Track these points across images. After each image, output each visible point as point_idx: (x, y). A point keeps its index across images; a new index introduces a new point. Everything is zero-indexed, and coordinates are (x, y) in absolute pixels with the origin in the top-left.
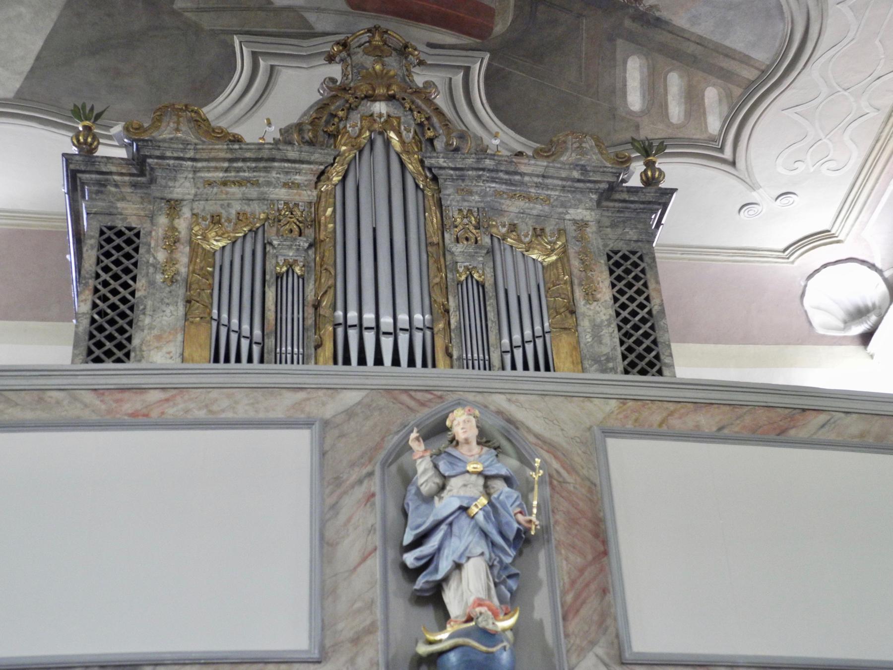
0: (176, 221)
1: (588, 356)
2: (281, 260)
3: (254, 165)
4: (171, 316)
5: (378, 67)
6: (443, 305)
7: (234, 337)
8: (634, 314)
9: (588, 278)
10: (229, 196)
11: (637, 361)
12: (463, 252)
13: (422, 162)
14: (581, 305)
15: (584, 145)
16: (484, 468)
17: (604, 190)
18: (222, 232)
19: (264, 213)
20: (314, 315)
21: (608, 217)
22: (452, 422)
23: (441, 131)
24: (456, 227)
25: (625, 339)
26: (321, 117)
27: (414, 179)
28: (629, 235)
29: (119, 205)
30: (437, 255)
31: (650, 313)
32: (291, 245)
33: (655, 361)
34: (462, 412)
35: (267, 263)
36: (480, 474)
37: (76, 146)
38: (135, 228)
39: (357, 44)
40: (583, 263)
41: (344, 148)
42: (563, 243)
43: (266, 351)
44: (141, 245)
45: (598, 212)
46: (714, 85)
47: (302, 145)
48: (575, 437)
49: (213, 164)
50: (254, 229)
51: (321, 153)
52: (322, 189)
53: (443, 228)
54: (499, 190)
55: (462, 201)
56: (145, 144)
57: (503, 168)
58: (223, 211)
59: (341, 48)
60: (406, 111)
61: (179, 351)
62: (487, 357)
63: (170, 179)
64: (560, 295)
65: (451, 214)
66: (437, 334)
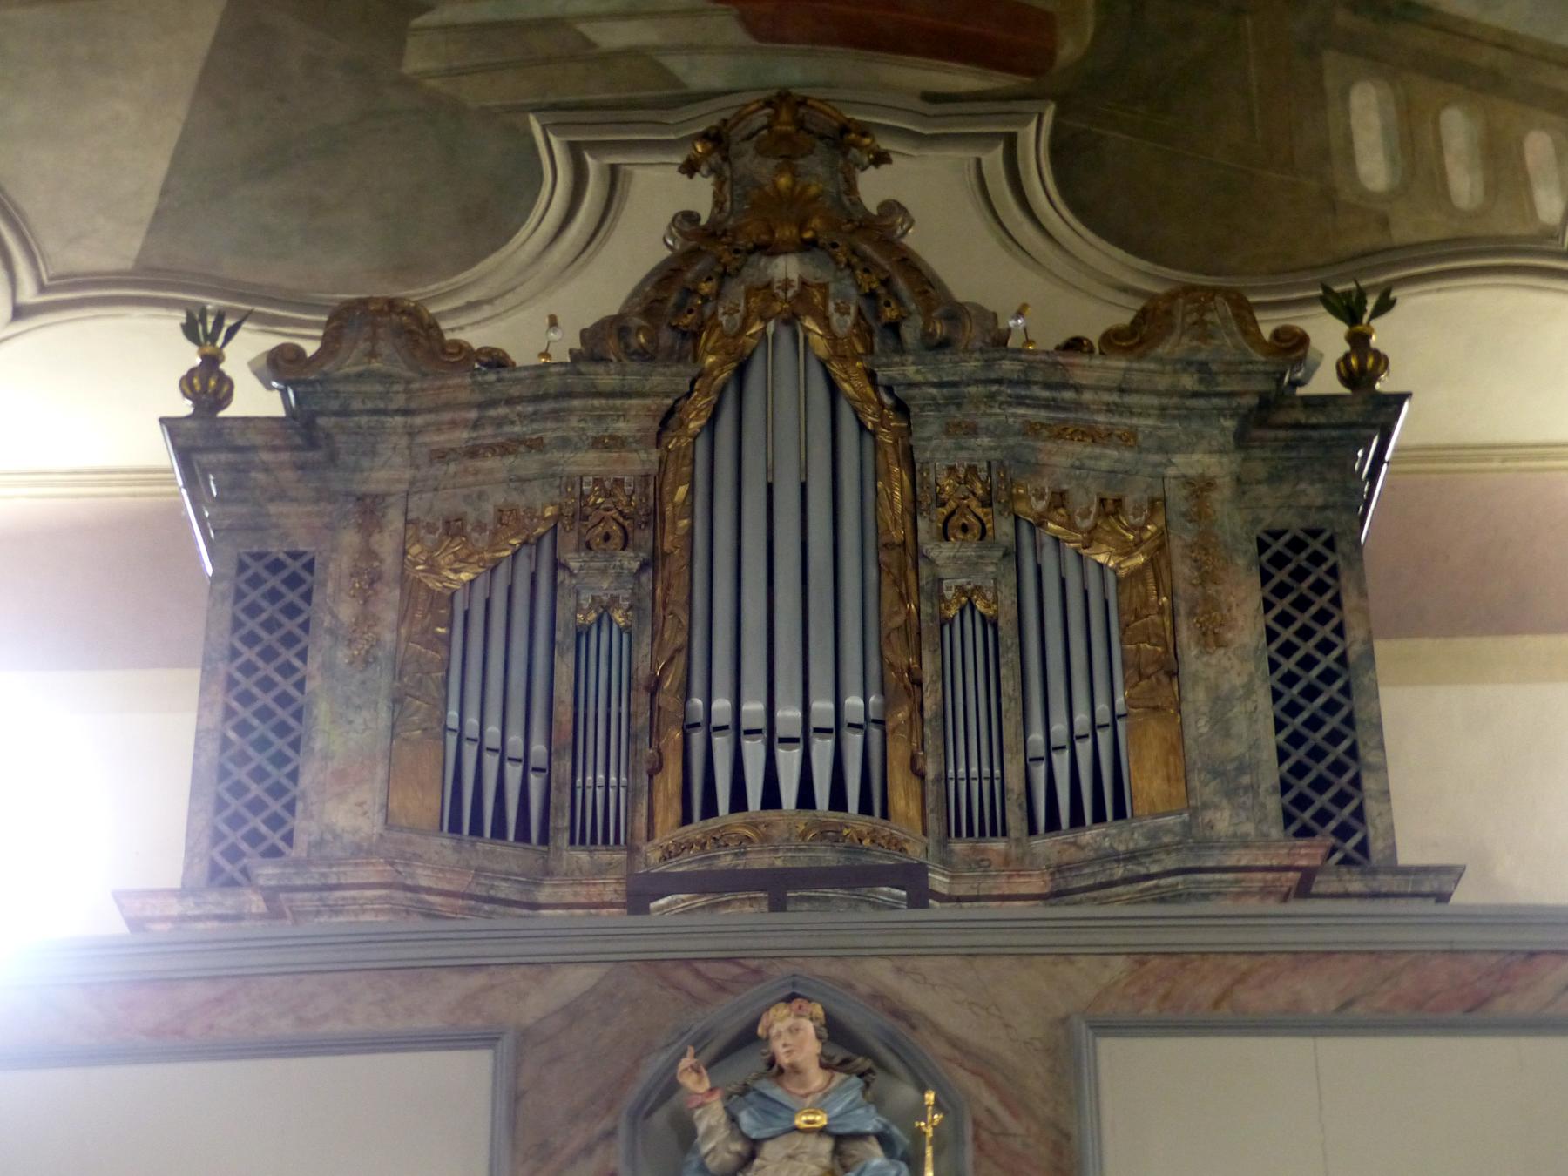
0: (376, 537)
1: (1199, 765)
2: (587, 599)
3: (530, 409)
4: (364, 730)
5: (784, 181)
6: (909, 670)
7: (491, 762)
8: (1308, 663)
9: (1207, 599)
10: (480, 477)
11: (1308, 762)
12: (954, 557)
13: (871, 376)
14: (1192, 657)
15: (1208, 317)
16: (829, 1120)
17: (1251, 410)
18: (466, 551)
19: (552, 505)
20: (648, 707)
21: (1264, 460)
22: (768, 1029)
23: (913, 307)
24: (943, 504)
25: (1287, 719)
26: (666, 299)
27: (856, 412)
28: (1306, 495)
29: (273, 508)
30: (900, 570)
31: (1342, 659)
32: (606, 568)
33: (1347, 760)
34: (786, 1011)
35: (559, 606)
36: (822, 1132)
37: (189, 398)
38: (303, 554)
39: (745, 133)
40: (1199, 569)
41: (711, 359)
42: (1160, 529)
43: (553, 784)
44: (315, 587)
45: (1238, 456)
46: (1543, 127)
47: (626, 361)
48: (1032, 1039)
49: (447, 416)
50: (532, 540)
51: (663, 374)
52: (670, 447)
53: (914, 508)
54: (1032, 421)
55: (955, 449)
56: (310, 389)
57: (1038, 377)
58: (469, 510)
59: (710, 145)
60: (841, 270)
61: (380, 798)
62: (997, 772)
63: (364, 454)
64: (1149, 639)
65: (932, 480)
66: (893, 731)
